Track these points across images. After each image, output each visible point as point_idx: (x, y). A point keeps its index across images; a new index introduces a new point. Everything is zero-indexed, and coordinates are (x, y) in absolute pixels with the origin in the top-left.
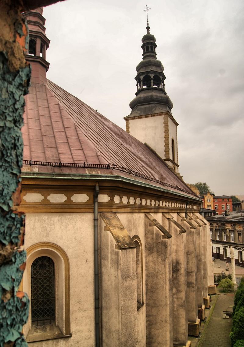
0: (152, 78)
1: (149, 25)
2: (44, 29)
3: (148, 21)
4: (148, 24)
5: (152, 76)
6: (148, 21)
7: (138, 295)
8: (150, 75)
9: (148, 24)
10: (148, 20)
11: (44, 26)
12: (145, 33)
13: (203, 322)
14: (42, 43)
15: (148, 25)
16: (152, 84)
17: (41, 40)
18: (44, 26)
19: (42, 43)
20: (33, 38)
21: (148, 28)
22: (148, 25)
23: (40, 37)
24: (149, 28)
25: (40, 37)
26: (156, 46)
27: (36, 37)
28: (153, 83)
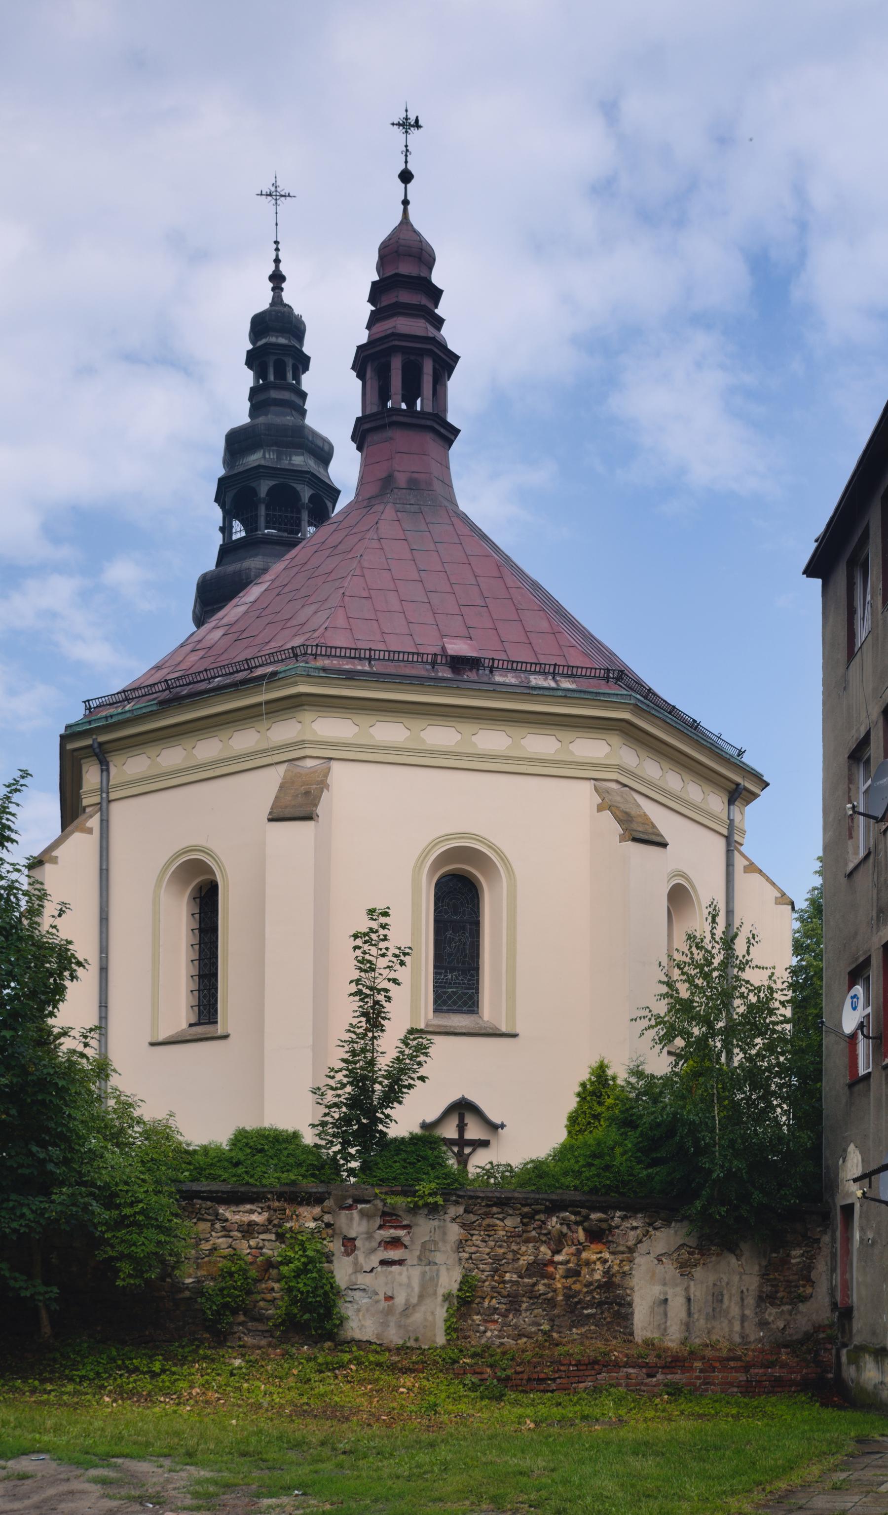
0: (307, 501)
1: (283, 268)
2: (438, 322)
3: (277, 250)
4: (277, 261)
5: (264, 487)
6: (277, 250)
7: (832, 1291)
8: (299, 487)
9: (277, 261)
10: (276, 242)
11: (436, 311)
12: (262, 301)
13: (337, 1334)
14: (437, 366)
15: (277, 267)
16: (262, 521)
17: (434, 361)
18: (373, 308)
19: (437, 366)
20: (412, 358)
21: (277, 279)
22: (277, 267)
23: (431, 353)
24: (282, 278)
25: (431, 353)
26: (447, 362)
27: (422, 353)
28: (267, 515)
